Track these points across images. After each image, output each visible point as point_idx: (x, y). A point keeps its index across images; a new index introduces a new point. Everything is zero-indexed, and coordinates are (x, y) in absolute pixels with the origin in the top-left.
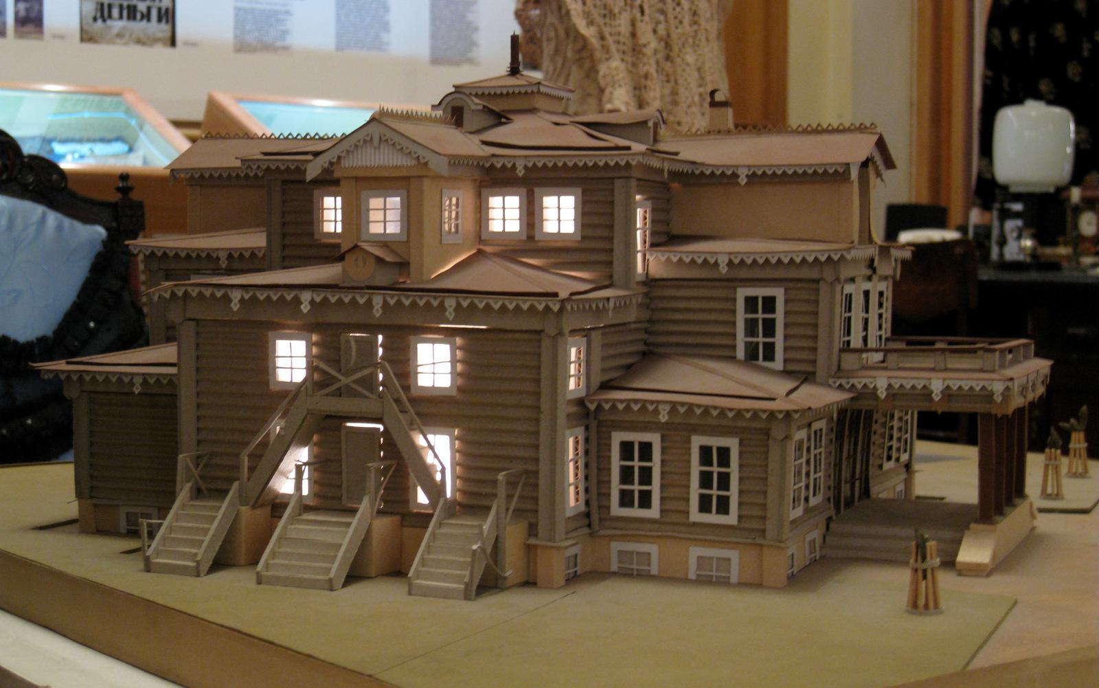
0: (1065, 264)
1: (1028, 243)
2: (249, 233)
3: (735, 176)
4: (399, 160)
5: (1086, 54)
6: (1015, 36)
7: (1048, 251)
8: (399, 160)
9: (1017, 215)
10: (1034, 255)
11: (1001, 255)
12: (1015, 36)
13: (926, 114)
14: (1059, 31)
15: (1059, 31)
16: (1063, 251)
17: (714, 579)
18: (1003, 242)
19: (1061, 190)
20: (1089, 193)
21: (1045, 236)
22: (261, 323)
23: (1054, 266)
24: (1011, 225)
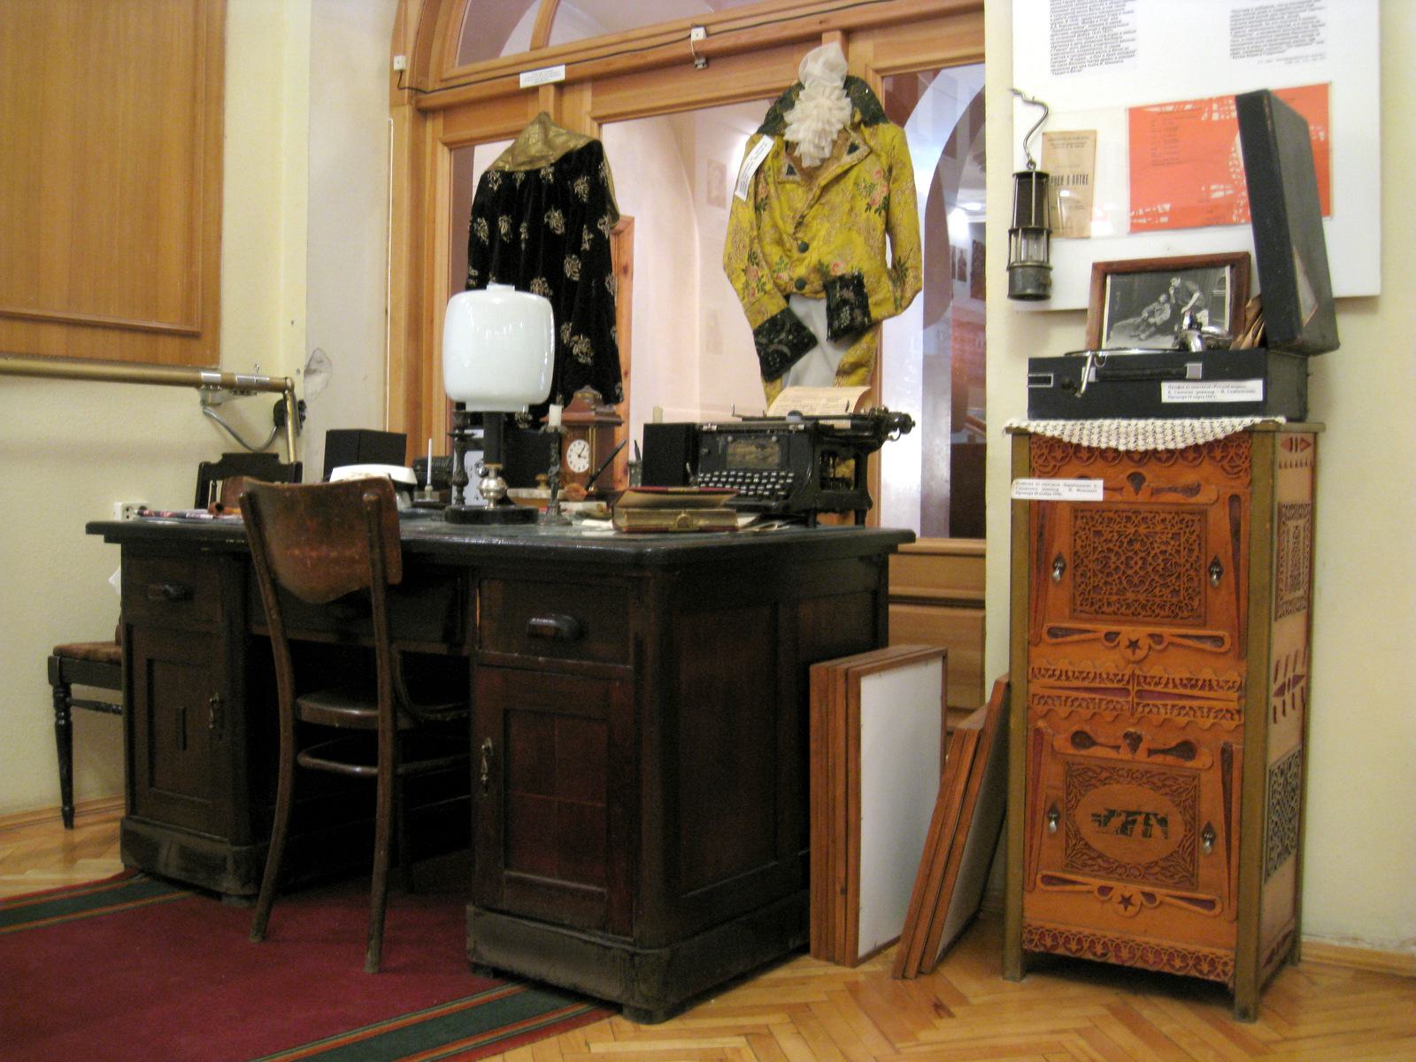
0: (543, 511)
1: (492, 484)
2: (1306, 58)
3: (765, 431)
4: (1077, 432)
5: (586, 246)
6: (504, 227)
7: (524, 493)
8: (1077, 432)
9: (477, 445)
10: (503, 500)
11: (461, 500)
12: (504, 227)
13: (403, 323)
14: (556, 220)
15: (556, 220)
16: (542, 493)
17: (63, 722)
18: (463, 483)
19: (539, 411)
20: (575, 416)
21: (516, 474)
22: (466, 141)
23: (528, 516)
24: (474, 458)
